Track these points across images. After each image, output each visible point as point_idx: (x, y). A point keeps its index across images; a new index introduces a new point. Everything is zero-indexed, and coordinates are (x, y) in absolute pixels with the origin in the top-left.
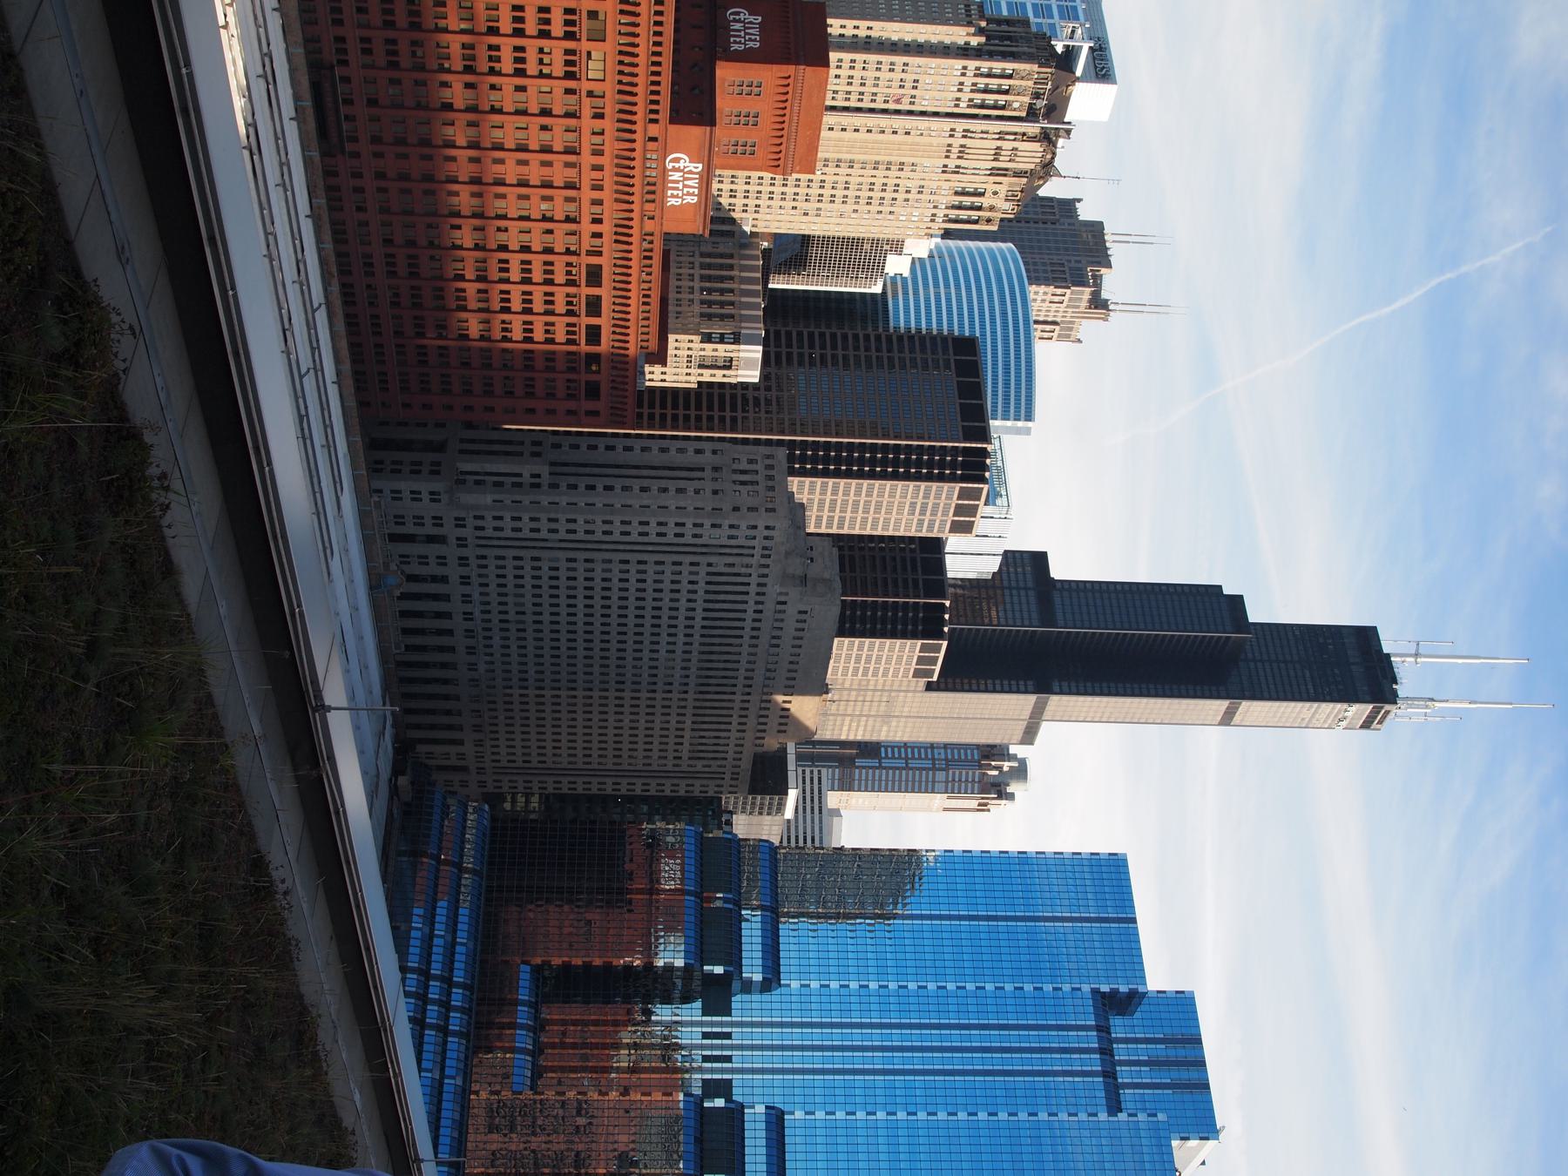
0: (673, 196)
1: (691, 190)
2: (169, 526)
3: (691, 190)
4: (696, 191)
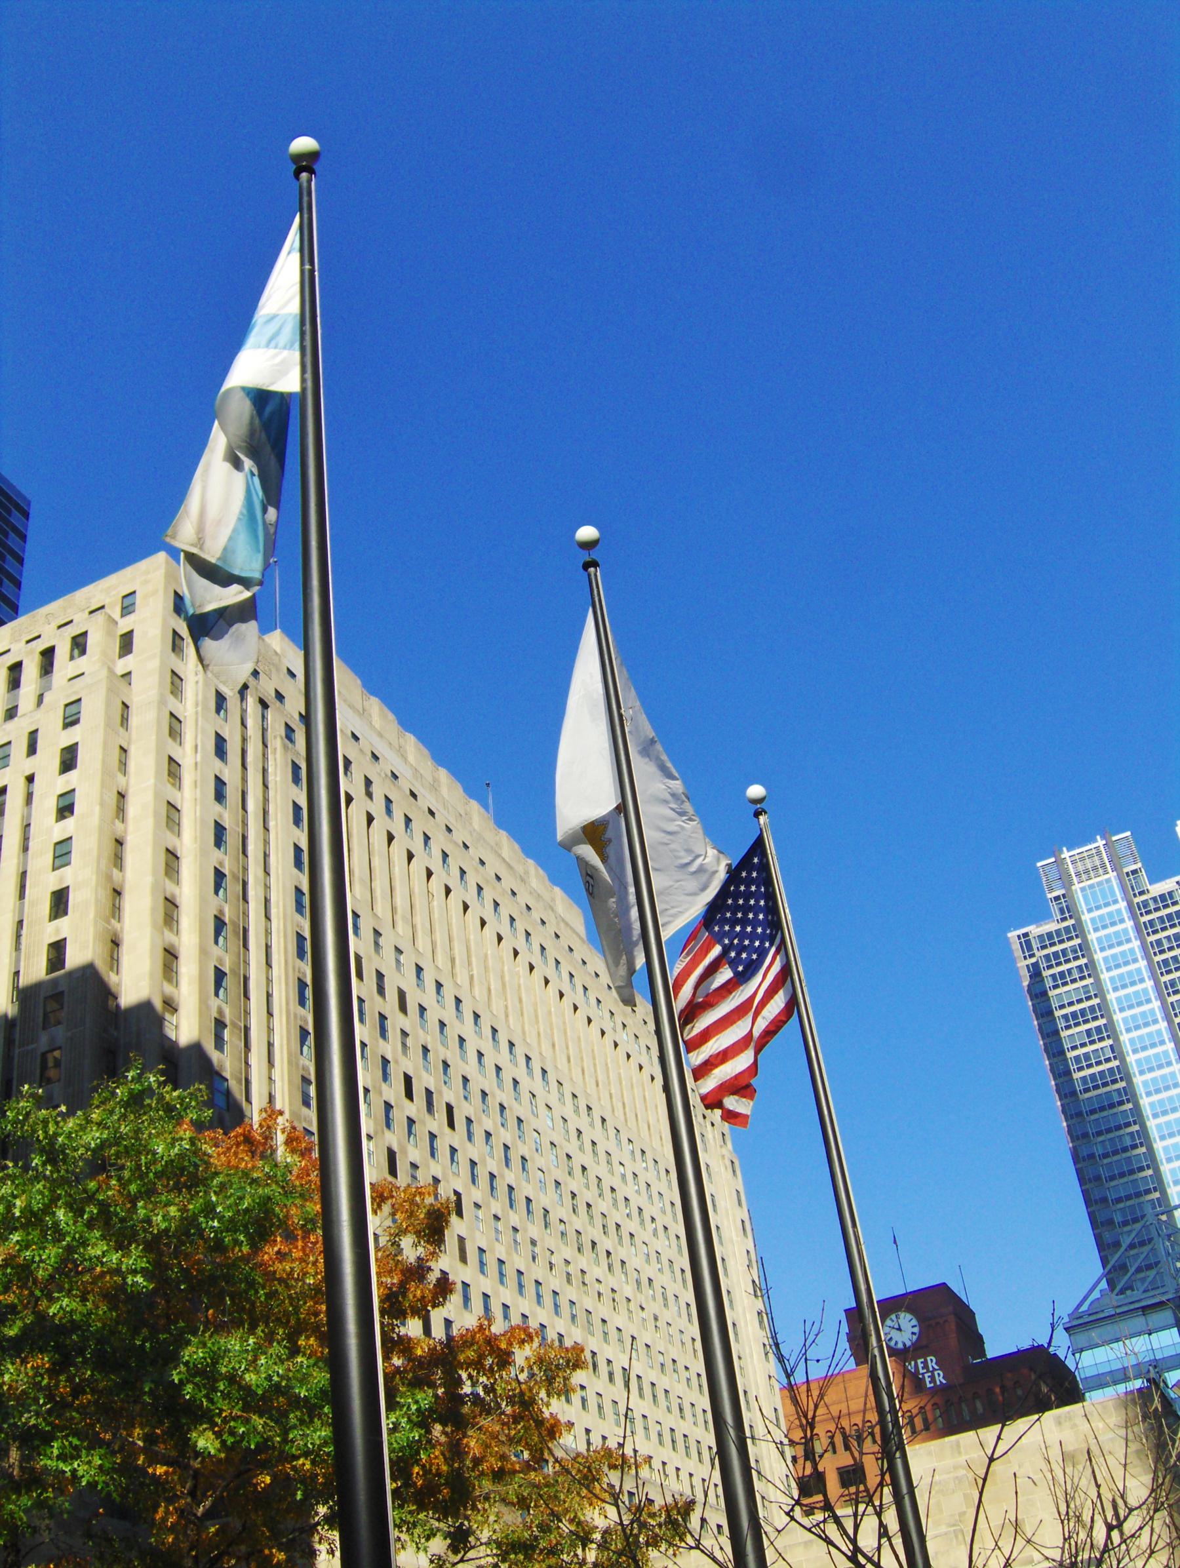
0: (932, 1378)
1: (920, 1366)
2: (913, 1333)
3: (920, 1366)
4: (919, 1361)
